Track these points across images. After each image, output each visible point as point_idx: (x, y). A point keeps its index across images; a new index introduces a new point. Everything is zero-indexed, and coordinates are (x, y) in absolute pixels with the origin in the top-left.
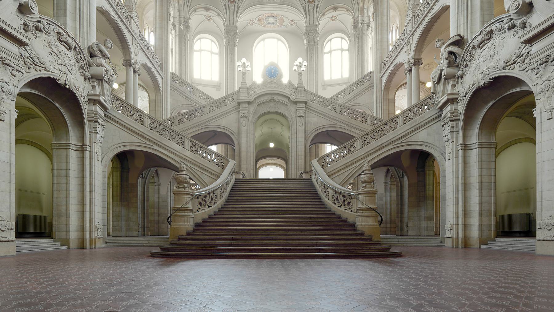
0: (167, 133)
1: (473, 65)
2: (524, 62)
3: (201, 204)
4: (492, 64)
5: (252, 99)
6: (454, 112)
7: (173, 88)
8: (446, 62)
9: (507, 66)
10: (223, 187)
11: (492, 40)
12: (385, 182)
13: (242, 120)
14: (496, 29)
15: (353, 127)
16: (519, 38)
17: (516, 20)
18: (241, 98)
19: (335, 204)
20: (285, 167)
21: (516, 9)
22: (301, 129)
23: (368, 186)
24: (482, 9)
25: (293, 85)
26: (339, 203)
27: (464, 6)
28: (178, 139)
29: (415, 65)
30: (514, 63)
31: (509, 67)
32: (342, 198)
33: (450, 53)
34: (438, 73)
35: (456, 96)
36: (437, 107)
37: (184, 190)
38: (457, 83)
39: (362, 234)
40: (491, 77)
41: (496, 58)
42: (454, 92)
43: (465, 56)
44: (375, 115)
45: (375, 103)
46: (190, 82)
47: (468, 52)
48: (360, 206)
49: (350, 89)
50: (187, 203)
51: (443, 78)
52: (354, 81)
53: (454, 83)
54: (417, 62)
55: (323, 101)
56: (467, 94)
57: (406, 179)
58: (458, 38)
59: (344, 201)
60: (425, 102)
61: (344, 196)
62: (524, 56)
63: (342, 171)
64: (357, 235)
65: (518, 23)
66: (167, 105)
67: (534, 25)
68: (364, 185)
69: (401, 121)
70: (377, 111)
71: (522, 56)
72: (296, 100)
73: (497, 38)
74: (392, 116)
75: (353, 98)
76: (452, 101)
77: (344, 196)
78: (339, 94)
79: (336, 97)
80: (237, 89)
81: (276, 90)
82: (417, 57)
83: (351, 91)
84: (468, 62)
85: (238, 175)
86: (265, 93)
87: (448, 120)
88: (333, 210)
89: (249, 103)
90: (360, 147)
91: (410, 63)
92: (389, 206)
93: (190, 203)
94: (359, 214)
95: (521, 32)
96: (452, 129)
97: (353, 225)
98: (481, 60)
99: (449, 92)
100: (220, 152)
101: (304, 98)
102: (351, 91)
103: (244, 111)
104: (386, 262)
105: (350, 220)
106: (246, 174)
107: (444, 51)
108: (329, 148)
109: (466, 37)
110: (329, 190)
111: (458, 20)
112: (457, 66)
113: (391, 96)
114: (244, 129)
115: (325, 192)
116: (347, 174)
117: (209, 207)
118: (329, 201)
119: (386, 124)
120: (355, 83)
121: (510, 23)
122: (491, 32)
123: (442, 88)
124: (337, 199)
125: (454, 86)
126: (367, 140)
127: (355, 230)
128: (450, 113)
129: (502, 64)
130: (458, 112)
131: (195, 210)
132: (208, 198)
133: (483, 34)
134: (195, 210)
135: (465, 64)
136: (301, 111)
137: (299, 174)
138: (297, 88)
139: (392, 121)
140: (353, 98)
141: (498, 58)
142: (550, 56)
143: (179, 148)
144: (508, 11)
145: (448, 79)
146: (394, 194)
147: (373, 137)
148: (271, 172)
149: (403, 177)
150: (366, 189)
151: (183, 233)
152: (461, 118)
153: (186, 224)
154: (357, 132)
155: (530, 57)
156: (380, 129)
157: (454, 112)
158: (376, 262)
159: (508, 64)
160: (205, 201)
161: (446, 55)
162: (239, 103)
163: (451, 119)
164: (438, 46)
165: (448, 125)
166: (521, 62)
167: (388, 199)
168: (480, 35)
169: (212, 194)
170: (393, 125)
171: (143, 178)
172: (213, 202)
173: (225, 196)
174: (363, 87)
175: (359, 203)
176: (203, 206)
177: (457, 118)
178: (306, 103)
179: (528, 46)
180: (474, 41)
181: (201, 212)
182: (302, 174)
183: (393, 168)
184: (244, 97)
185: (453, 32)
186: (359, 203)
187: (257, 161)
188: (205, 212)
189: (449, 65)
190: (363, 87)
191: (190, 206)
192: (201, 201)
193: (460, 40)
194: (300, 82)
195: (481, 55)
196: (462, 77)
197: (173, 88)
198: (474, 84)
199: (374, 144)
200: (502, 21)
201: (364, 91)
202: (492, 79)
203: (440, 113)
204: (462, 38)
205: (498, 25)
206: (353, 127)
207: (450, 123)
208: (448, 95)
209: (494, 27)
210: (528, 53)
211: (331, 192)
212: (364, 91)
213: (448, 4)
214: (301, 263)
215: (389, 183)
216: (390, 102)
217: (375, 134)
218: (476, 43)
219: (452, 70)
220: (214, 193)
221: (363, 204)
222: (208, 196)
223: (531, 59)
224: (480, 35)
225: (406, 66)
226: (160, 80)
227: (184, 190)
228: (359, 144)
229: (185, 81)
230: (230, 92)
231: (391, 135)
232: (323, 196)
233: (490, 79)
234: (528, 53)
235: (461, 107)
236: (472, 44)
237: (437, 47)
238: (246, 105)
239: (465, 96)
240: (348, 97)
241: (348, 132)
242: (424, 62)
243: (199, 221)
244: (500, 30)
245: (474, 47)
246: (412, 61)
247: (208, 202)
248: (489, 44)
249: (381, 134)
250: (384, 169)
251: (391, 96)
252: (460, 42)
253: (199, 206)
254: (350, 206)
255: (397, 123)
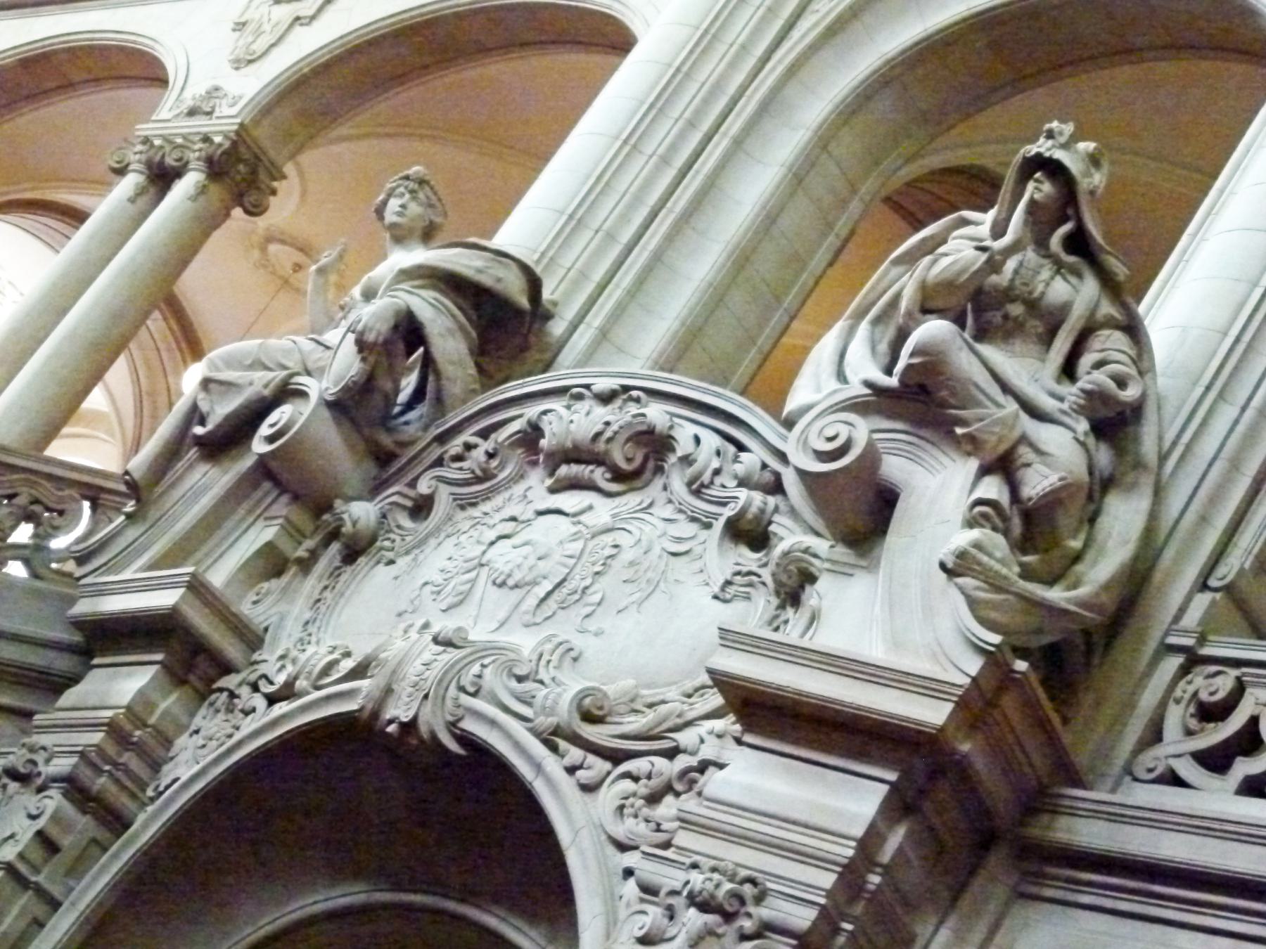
1: (448, 547)
2: (654, 799)
4: (525, 643)
6: (140, 749)
8: (344, 364)
9: (577, 740)
11: (632, 500)
14: (687, 460)
16: (728, 638)
17: (793, 513)
21: (823, 456)
24: (741, 260)
27: (682, 136)
29: (217, 168)
30: (616, 757)
31: (575, 754)
33: (409, 332)
34: (259, 383)
35: (231, 649)
36: (84, 607)
38: (306, 565)
40: (469, 725)
41: (565, 628)
42: (245, 608)
43: (455, 446)
47: (484, 434)
51: (259, 446)
53: (286, 546)
54: (240, 173)
56: (287, 692)
58: (514, 287)
60: (47, 491)
62: (682, 762)
65: (790, 536)
67: (827, 638)
71: (671, 754)
73: (649, 522)
76: (192, 654)
82: (262, 134)
84: (444, 497)
87: (62, 765)
91: (200, 124)
95: (753, 613)
96: (37, 855)
98: (504, 557)
99: (218, 577)
107: (388, 281)
109: (557, 328)
111: (602, 184)
112: (383, 458)
121: (758, 498)
122: (655, 445)
123: (206, 502)
125: (272, 564)
128: (113, 728)
129: (560, 696)
130: (156, 767)
133: (618, 416)
135: (424, 487)
141: (578, 641)
142: (759, 899)
144: (789, 424)
145: (281, 487)
152: (147, 826)
155: (689, 803)
157: (140, 749)
159: (586, 731)
161: (373, 315)
163: (86, 774)
164: (390, 217)
165: (30, 801)
166: (642, 788)
168: (606, 398)
177: (124, 802)
179: (729, 724)
180: (557, 405)
185: (522, 230)
189: (352, 405)
193: (518, 312)
195: (536, 527)
196: (352, 554)
198: (359, 672)
200: (741, 447)
202: (466, 740)
203: (62, 663)
204: (540, 313)
205: (711, 441)
207: (54, 800)
208: (196, 587)
209: (684, 434)
210: (703, 767)
213: (636, 26)
214: (189, 311)
218: (569, 422)
219: (334, 448)
223: (685, 822)
224: (606, 398)
225: (165, 118)
233: (452, 726)
234: (703, 767)
235: (204, 749)
236: (531, 411)
237: (380, 212)
239: (272, 700)
242: (284, 208)
244: (697, 488)
245: (530, 438)
246: (224, 123)
248: (602, 510)
252: (506, 325)
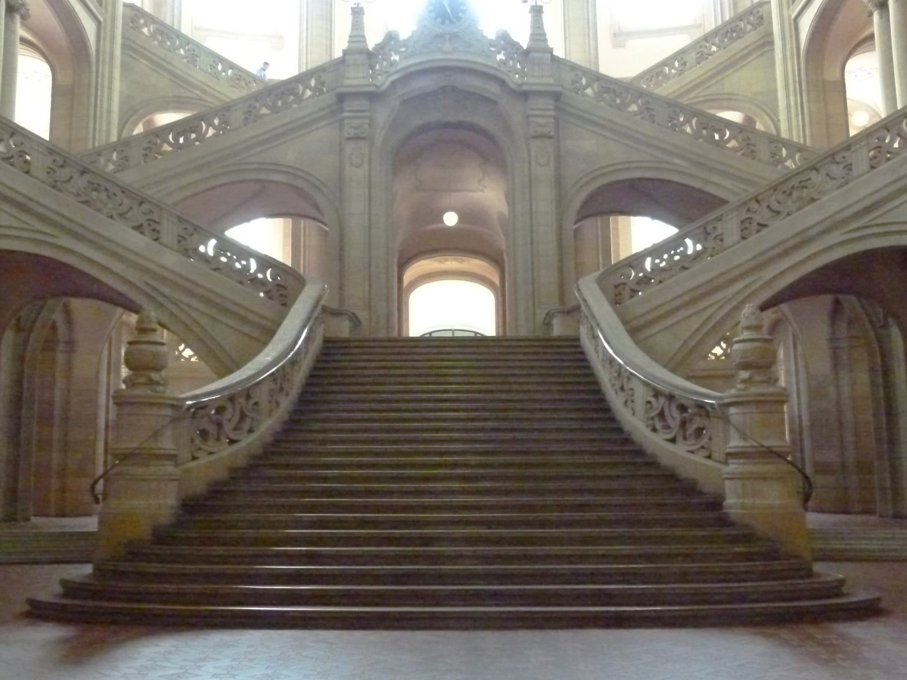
0: (104, 195)
3: (204, 434)
5: (383, 82)
7: (131, 49)
10: (280, 378)
12: (833, 339)
13: (349, 147)
15: (711, 169)
18: (346, 82)
19: (654, 430)
20: (497, 281)
22: (545, 173)
23: (757, 378)
25: (515, 45)
26: (667, 427)
28: (137, 215)
32: (676, 414)
37: (149, 392)
39: (748, 537)
44: (784, 135)
45: (781, 94)
46: (186, 30)
48: (735, 443)
49: (699, 49)
50: (156, 435)
52: (711, 26)
55: (612, 89)
57: (895, 333)
59: (683, 424)
61: (683, 408)
63: (682, 314)
64: (735, 540)
66: (110, 99)
68: (744, 374)
69: (861, 158)
70: (789, 120)
72: (525, 88)
74: (836, 141)
75: (711, 77)
77: (683, 408)
78: (664, 63)
79: (656, 72)
80: (338, 54)
81: (461, 57)
83: (702, 57)
85: (334, 322)
86: (427, 66)
88: (649, 449)
89: (373, 97)
90: (736, 237)
92: (848, 416)
93: (169, 432)
94: (734, 467)
97: (716, 503)
100: (280, 252)
101: (551, 81)
102: (702, 57)
103: (357, 122)
104: (820, 643)
105: (707, 486)
106: (363, 315)
108: (642, 233)
110: (635, 384)
113: (831, 75)
114: (356, 174)
115: (622, 389)
116: (696, 323)
117: (232, 442)
118: (634, 420)
119: (816, 170)
120: (715, 33)
124: (661, 415)
126: (758, 218)
127: (724, 522)
131: (185, 454)
132: (228, 414)
134: (185, 454)
136: (541, 121)
137: (541, 315)
138: (526, 53)
139: (837, 154)
140: (711, 77)
143: (137, 241)
146: (863, 377)
147: (775, 206)
148: (451, 305)
149: (885, 326)
150: (753, 390)
151: (143, 530)
153: (153, 502)
154: (728, 183)
156: (794, 182)
158: (786, 643)
160: (219, 425)
162: (341, 98)
167: (846, 391)
169: (242, 400)
170: (836, 170)
171: (18, 329)
172: (246, 426)
173: (286, 403)
174: (738, 45)
175: (733, 433)
176: (211, 442)
178: (557, 96)
181: (204, 460)
182: (549, 316)
183: (853, 298)
184: (355, 79)
186: (733, 433)
187: (403, 264)
188: (218, 459)
190: (738, 45)
191: (167, 444)
192: (205, 424)
194: (538, 34)
197: (131, 49)
199: (781, 230)
201: (746, 55)
206: (711, 169)
211: (641, 394)
212: (746, 55)
215: (844, 344)
216: (829, 93)
217: (781, 198)
220: (248, 397)
221: (743, 436)
222: (229, 406)
226: (89, 27)
227: (149, 392)
228: (730, 228)
229: (171, 29)
230: (317, 59)
231: (833, 202)
232: (616, 401)
238: (363, 103)
240: (694, 74)
241: (697, 184)
243: (199, 487)
247: (228, 427)
249: (799, 198)
250: (827, 300)
251: (831, 75)
253: (198, 441)
254: (704, 441)
255: (849, 167)
